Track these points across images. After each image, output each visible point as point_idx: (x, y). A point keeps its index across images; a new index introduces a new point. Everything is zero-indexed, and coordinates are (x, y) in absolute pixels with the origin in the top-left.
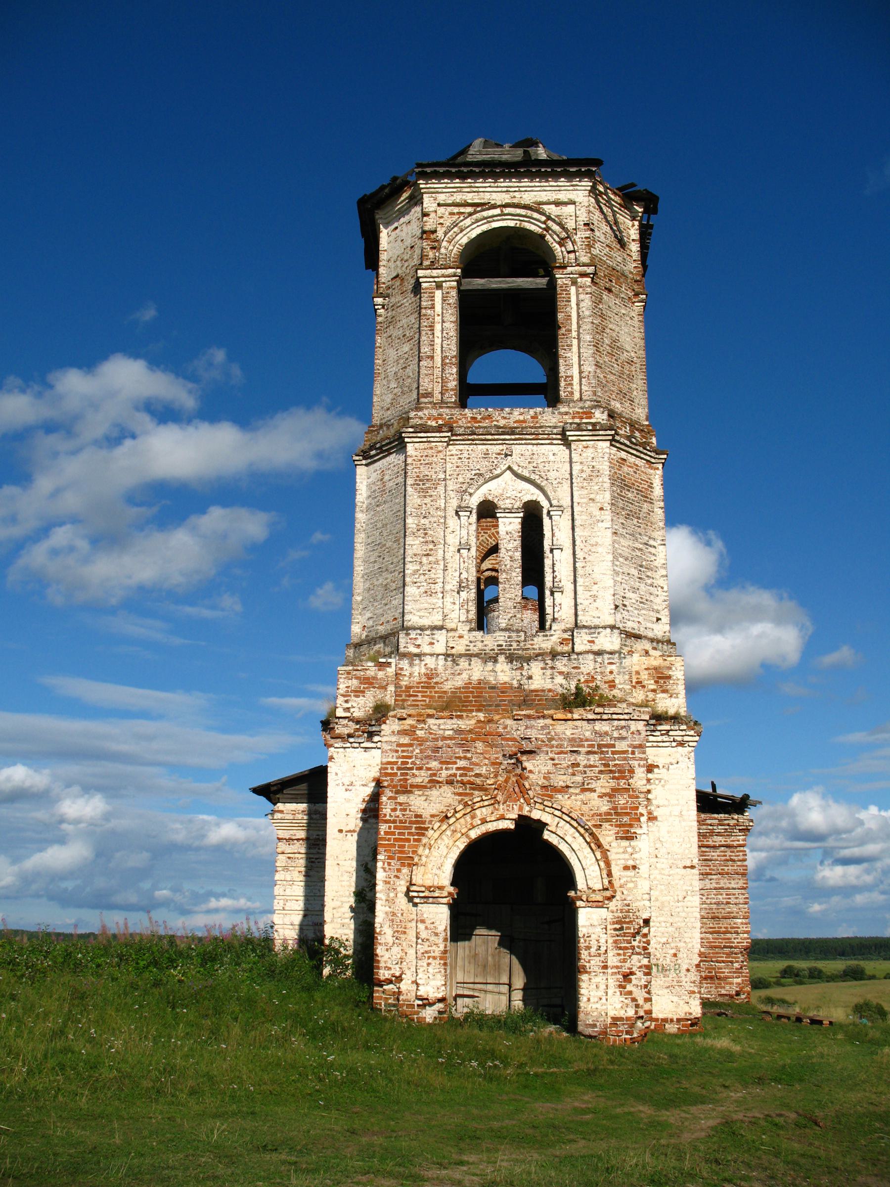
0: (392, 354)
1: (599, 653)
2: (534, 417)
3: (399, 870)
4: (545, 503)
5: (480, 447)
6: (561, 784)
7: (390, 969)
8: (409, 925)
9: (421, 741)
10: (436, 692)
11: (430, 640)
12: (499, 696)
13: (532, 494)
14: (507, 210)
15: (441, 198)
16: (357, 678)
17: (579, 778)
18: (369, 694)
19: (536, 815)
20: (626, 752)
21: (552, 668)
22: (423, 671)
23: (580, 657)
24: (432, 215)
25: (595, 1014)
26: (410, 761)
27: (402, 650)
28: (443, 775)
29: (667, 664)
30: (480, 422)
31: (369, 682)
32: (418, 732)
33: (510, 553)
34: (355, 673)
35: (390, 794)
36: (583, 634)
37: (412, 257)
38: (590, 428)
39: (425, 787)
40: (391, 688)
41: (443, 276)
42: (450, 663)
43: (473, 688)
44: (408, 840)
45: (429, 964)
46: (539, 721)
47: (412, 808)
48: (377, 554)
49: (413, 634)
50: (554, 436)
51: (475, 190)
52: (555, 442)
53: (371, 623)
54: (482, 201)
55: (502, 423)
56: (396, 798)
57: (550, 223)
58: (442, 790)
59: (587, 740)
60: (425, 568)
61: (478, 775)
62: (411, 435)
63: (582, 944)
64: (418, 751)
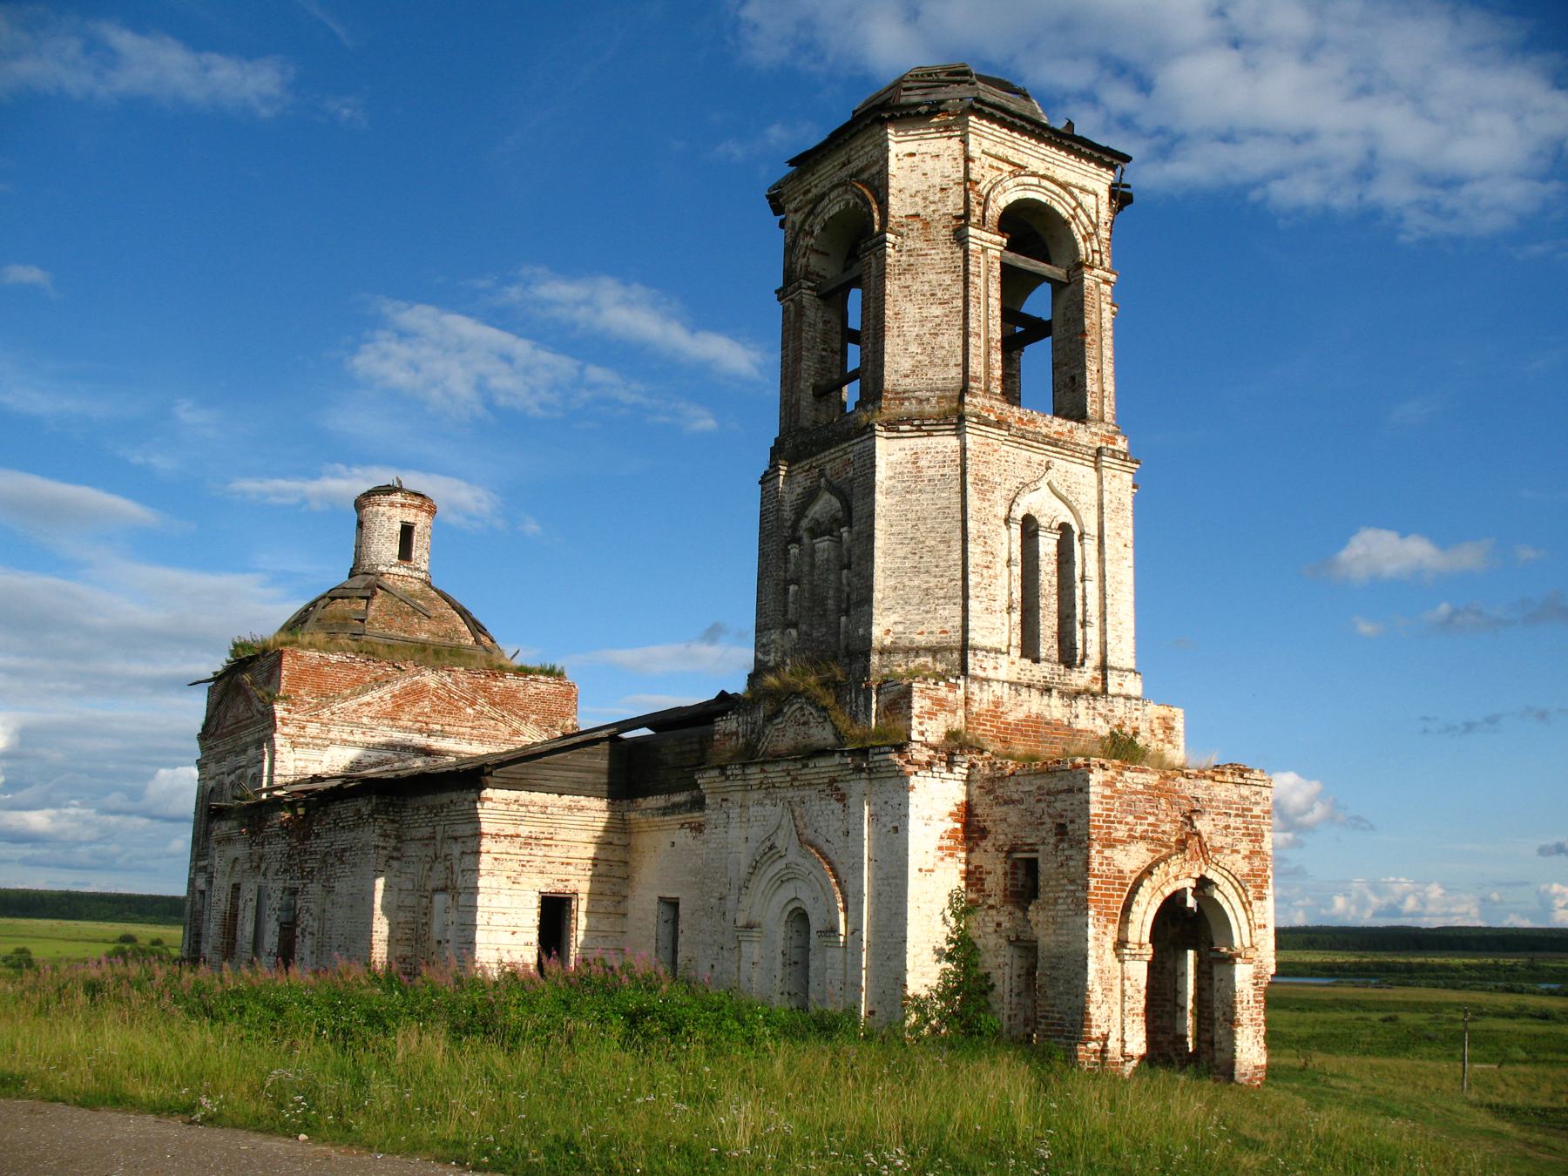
0: (911, 311)
1: (1128, 698)
2: (1070, 431)
3: (1106, 927)
4: (1076, 529)
5: (1024, 452)
6: (1219, 845)
7: (1100, 1027)
8: (1114, 982)
9: (1121, 794)
10: (1002, 723)
11: (995, 664)
12: (1052, 733)
13: (1066, 516)
14: (1045, 183)
15: (986, 144)
16: (931, 698)
17: (1229, 840)
18: (941, 717)
19: (1210, 875)
20: (1258, 817)
21: (1094, 708)
22: (991, 698)
23: (1115, 699)
24: (977, 162)
25: (1246, 1064)
26: (1112, 814)
27: (970, 672)
28: (1138, 831)
29: (1171, 714)
30: (1025, 425)
31: (940, 703)
32: (1118, 784)
33: (1049, 577)
34: (928, 691)
35: (1098, 848)
36: (1114, 676)
37: (943, 201)
38: (1122, 457)
39: (1124, 842)
40: (961, 713)
41: (991, 242)
42: (1013, 692)
43: (1032, 722)
44: (1112, 896)
45: (1133, 1021)
46: (1204, 781)
47: (1116, 862)
48: (908, 549)
49: (980, 654)
50: (1087, 457)
51: (1017, 147)
52: (1086, 463)
53: (900, 628)
54: (1021, 163)
55: (1044, 431)
56: (1102, 852)
57: (1079, 211)
58: (1138, 845)
59: (1235, 803)
60: (985, 581)
61: (1164, 832)
62: (974, 425)
63: (1238, 999)
64: (1117, 804)
